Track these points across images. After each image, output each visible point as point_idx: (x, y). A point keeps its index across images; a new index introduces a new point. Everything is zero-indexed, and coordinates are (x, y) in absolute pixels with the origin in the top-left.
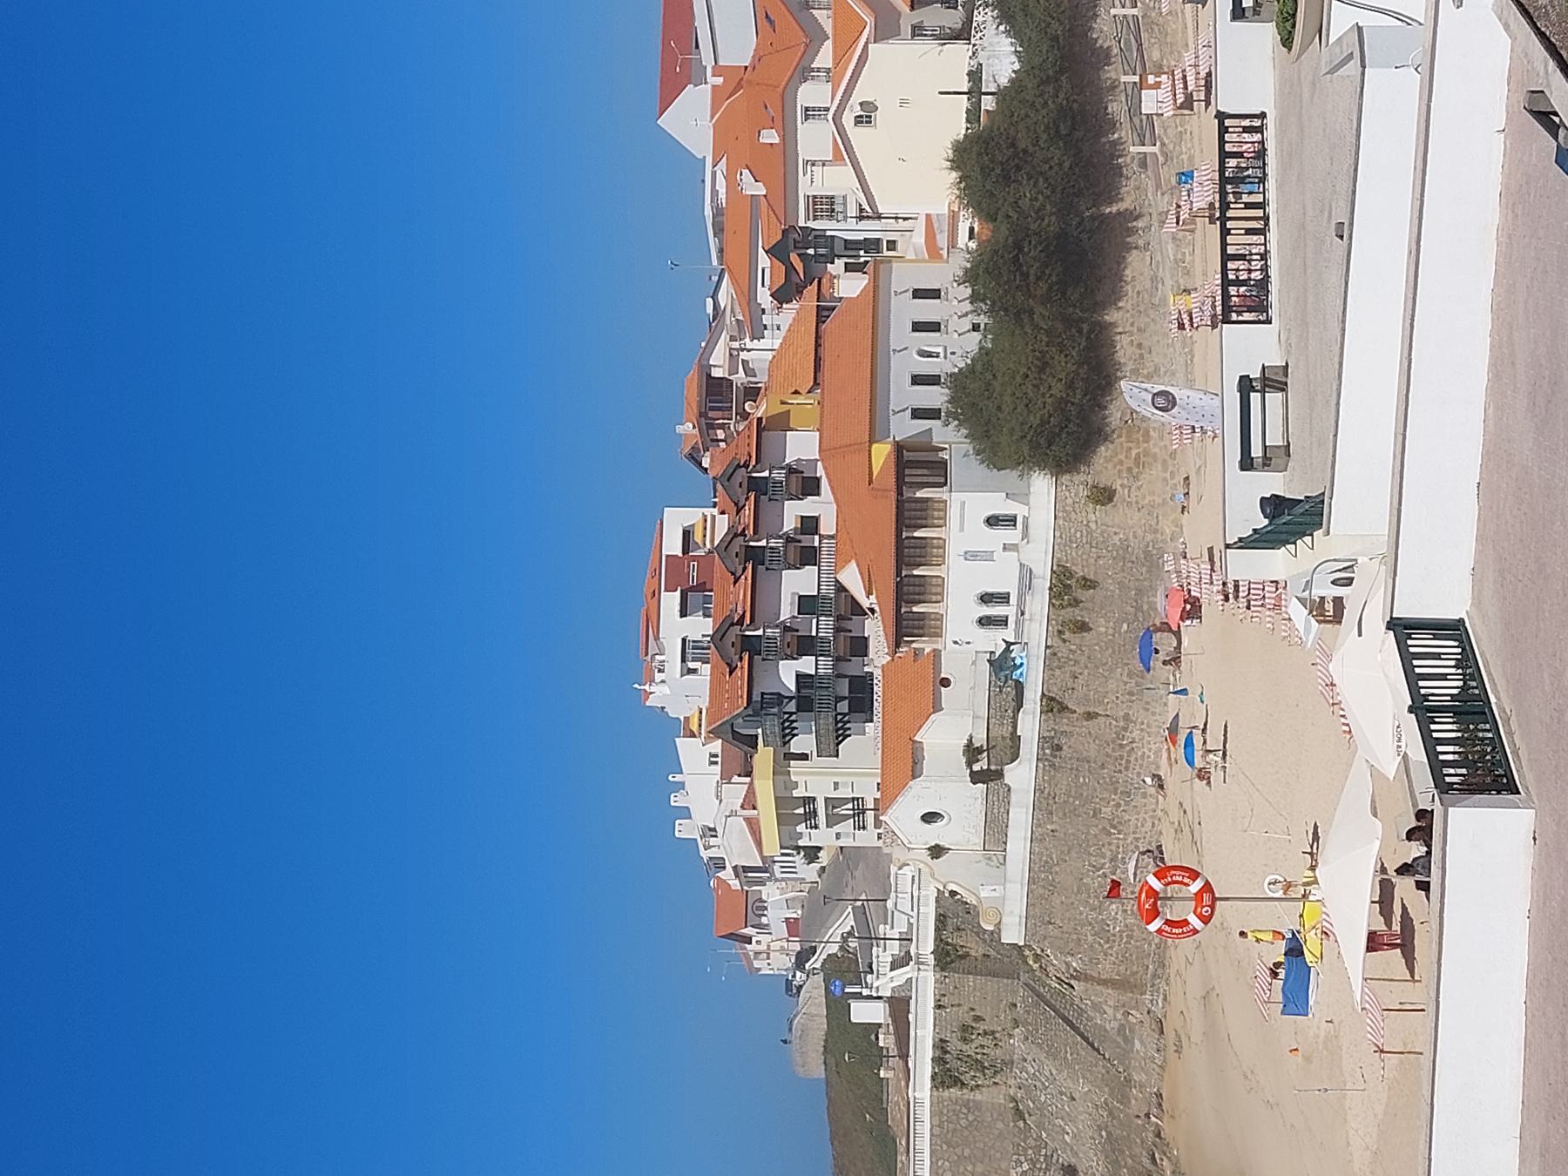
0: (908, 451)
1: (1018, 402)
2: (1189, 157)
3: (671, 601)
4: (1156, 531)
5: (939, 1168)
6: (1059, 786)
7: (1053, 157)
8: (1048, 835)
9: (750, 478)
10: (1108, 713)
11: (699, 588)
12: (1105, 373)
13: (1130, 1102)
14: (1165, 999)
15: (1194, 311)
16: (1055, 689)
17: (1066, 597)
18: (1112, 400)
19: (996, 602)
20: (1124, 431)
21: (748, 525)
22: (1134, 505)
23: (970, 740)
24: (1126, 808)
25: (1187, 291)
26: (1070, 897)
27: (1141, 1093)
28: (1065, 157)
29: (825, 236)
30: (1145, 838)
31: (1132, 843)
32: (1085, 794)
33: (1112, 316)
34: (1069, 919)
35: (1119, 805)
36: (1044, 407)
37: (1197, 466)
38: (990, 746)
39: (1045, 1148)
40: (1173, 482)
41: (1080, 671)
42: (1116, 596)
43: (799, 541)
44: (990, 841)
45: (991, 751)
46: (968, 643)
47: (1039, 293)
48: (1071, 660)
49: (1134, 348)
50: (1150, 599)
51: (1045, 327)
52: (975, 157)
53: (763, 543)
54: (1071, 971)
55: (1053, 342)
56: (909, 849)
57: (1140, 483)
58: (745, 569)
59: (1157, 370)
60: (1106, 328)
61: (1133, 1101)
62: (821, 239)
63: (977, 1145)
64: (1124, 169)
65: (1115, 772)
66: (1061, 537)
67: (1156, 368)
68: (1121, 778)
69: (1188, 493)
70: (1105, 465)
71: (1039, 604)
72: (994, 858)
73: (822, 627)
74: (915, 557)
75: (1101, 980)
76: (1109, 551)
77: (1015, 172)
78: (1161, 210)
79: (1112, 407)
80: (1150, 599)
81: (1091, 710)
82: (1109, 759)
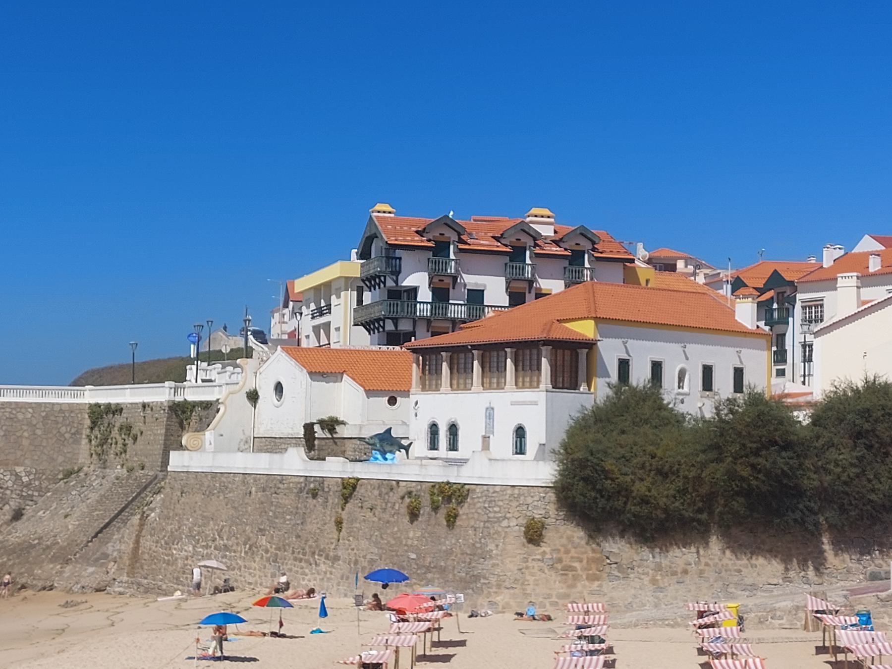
0: (587, 354)
1: (628, 448)
2: (886, 625)
4: (499, 586)
6: (284, 497)
7: (881, 483)
8: (248, 488)
9: (583, 253)
10: (341, 541)
12: (656, 535)
13: (52, 563)
14: (120, 593)
15: (717, 630)
16: (362, 491)
17: (440, 498)
18: (631, 544)
19: (450, 439)
20: (598, 555)
21: (543, 250)
22: (524, 565)
23: (343, 423)
24: (264, 558)
25: (741, 621)
26: (200, 510)
27: (57, 573)
28: (881, 496)
29: (789, 317)
30: (241, 576)
31: (237, 564)
32: (277, 521)
33: (715, 544)
34: (184, 509)
35: (267, 551)
36: (621, 474)
37: (556, 630)
38: (336, 440)
39: (39, 495)
40: (548, 604)
41: (377, 513)
42: (440, 547)
44: (261, 442)
45: (332, 441)
46: (416, 415)
47: (739, 468)
48: (386, 505)
49: (683, 566)
50: (436, 581)
51: (704, 475)
52: (880, 403)
53: (528, 261)
54: (148, 513)
55: (688, 483)
56: (256, 373)
57: (546, 571)
58: (506, 246)
59: (661, 589)
60: (702, 538)
61: (51, 566)
62: (786, 313)
63: (44, 440)
64: (868, 558)
65: (293, 548)
66: (495, 492)
67: (661, 588)
68: (288, 554)
69: (534, 619)
70: (565, 536)
71: (436, 474)
72: (247, 446)
73: (457, 309)
74: (490, 362)
75: (139, 538)
76: (480, 539)
77: (865, 444)
78: (828, 594)
79: (623, 543)
80: (436, 581)
81: (344, 525)
82: (303, 542)
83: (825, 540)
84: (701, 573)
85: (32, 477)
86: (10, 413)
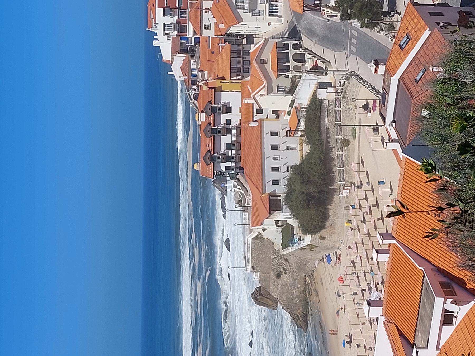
3: (160, 11)
5: (253, 256)
11: (168, 7)
43: (226, 127)
72: (278, 231)
73: (232, 153)
83: (330, 187)
84: (335, 210)
85: (274, 254)
86: (254, 260)
